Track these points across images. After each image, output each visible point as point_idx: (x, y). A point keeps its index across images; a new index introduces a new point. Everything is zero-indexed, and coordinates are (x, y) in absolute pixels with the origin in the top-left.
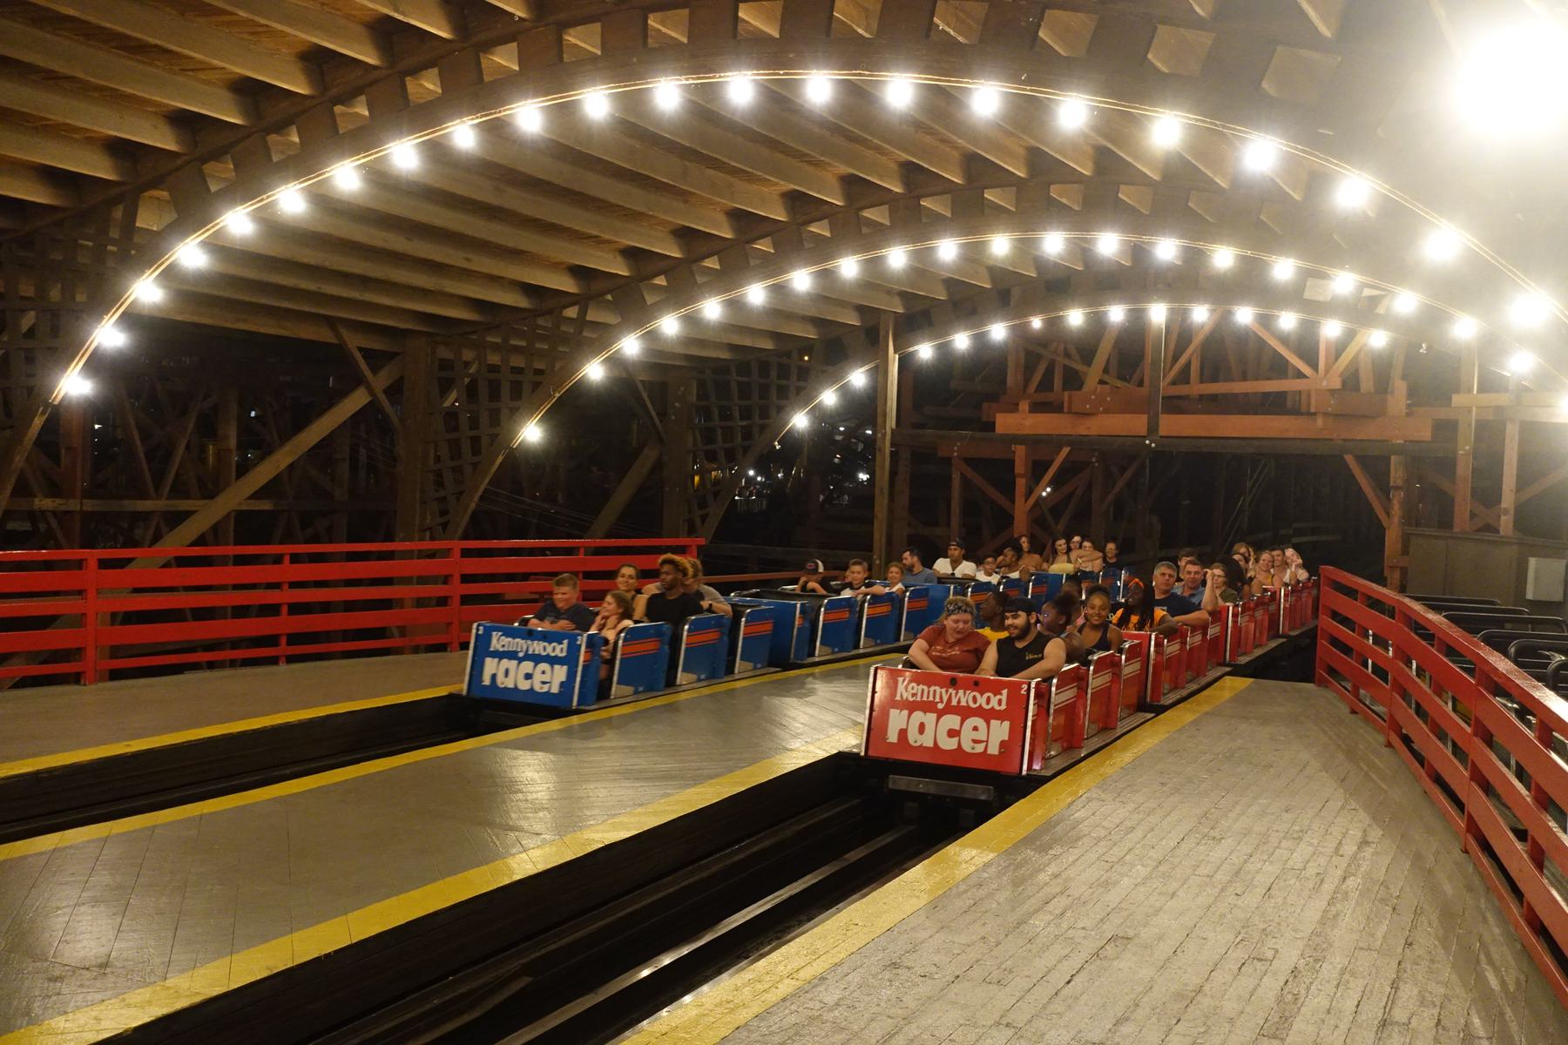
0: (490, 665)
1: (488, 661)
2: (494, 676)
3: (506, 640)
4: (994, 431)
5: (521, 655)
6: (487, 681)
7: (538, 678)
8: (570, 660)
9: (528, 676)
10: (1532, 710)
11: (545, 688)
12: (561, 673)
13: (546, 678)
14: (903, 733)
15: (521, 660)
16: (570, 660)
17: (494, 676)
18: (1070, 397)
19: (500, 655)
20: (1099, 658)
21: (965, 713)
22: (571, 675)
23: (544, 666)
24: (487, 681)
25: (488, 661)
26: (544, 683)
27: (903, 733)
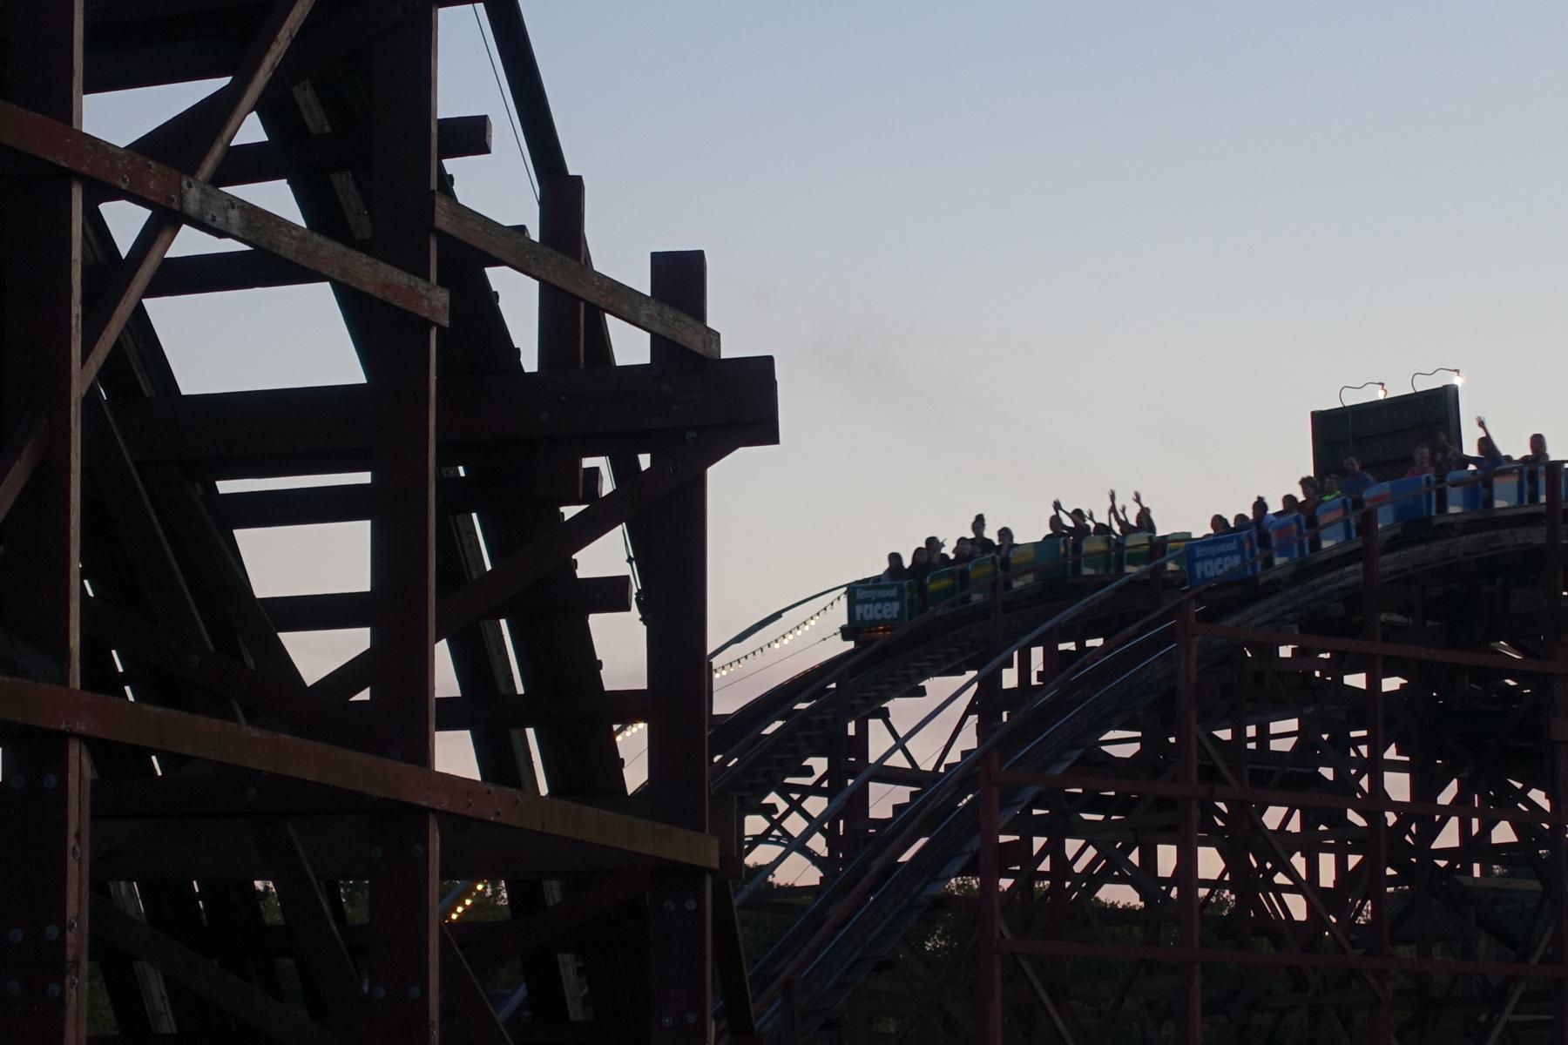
0: (1199, 567)
1: (857, 607)
2: (862, 615)
3: (864, 592)
4: (86, 92)
5: (1213, 555)
6: (858, 618)
7: (885, 611)
8: (900, 598)
9: (880, 611)
10: (86, 365)
11: (890, 616)
12: (896, 606)
13: (889, 610)
14: (1203, 573)
15: (1214, 558)
16: (900, 598)
17: (862, 615)
18: (1534, 498)
19: (1202, 559)
20: (82, 560)
21: (1222, 555)
22: (902, 606)
23: (887, 604)
24: (858, 618)
25: (857, 607)
26: (889, 613)
27: (1203, 573)
